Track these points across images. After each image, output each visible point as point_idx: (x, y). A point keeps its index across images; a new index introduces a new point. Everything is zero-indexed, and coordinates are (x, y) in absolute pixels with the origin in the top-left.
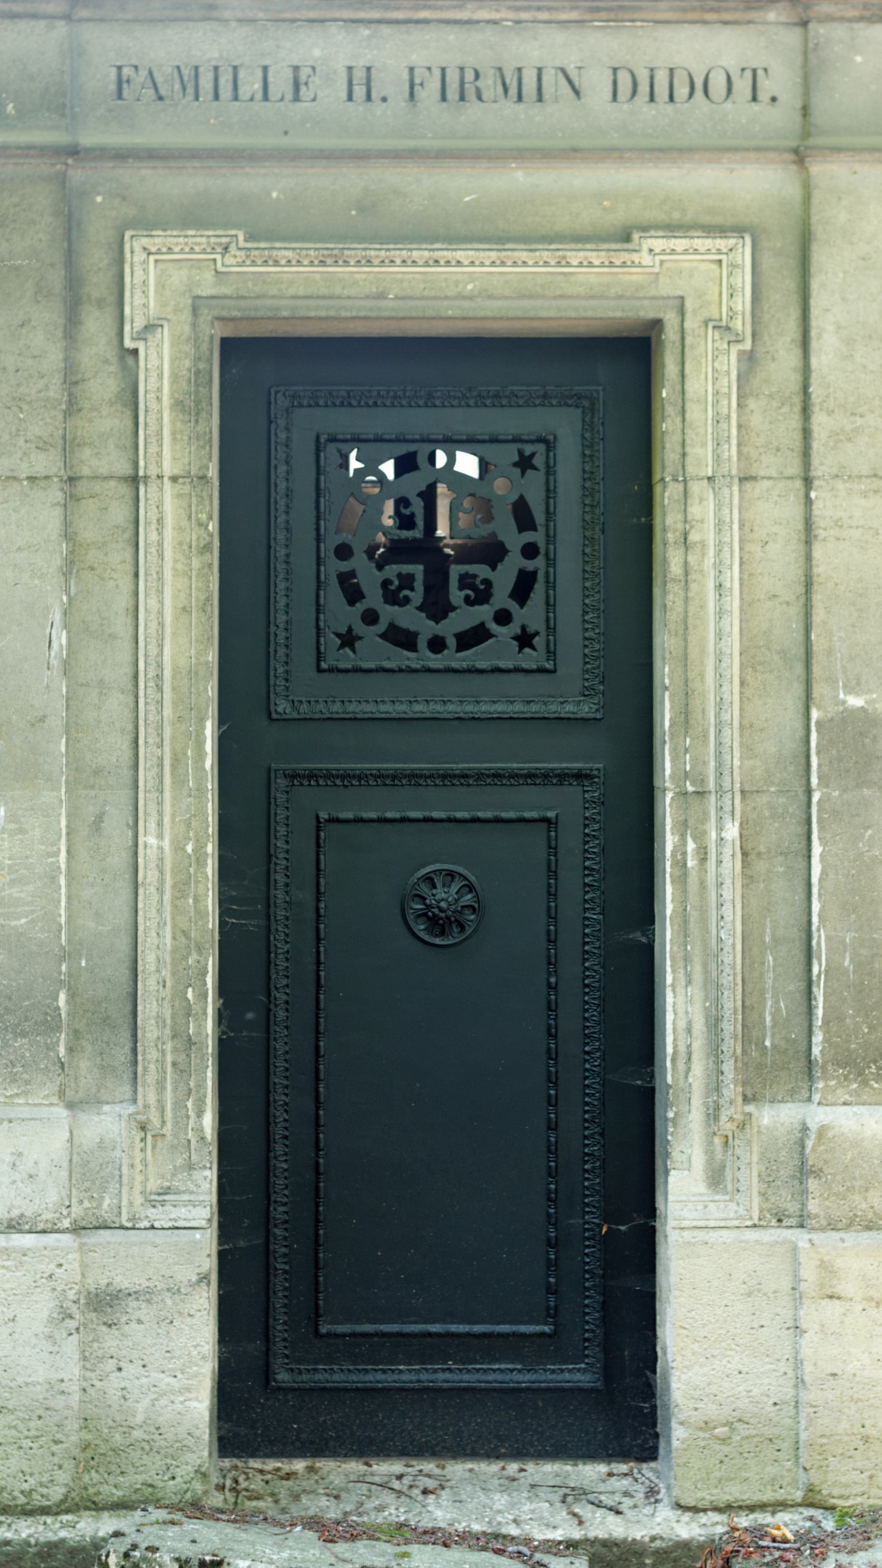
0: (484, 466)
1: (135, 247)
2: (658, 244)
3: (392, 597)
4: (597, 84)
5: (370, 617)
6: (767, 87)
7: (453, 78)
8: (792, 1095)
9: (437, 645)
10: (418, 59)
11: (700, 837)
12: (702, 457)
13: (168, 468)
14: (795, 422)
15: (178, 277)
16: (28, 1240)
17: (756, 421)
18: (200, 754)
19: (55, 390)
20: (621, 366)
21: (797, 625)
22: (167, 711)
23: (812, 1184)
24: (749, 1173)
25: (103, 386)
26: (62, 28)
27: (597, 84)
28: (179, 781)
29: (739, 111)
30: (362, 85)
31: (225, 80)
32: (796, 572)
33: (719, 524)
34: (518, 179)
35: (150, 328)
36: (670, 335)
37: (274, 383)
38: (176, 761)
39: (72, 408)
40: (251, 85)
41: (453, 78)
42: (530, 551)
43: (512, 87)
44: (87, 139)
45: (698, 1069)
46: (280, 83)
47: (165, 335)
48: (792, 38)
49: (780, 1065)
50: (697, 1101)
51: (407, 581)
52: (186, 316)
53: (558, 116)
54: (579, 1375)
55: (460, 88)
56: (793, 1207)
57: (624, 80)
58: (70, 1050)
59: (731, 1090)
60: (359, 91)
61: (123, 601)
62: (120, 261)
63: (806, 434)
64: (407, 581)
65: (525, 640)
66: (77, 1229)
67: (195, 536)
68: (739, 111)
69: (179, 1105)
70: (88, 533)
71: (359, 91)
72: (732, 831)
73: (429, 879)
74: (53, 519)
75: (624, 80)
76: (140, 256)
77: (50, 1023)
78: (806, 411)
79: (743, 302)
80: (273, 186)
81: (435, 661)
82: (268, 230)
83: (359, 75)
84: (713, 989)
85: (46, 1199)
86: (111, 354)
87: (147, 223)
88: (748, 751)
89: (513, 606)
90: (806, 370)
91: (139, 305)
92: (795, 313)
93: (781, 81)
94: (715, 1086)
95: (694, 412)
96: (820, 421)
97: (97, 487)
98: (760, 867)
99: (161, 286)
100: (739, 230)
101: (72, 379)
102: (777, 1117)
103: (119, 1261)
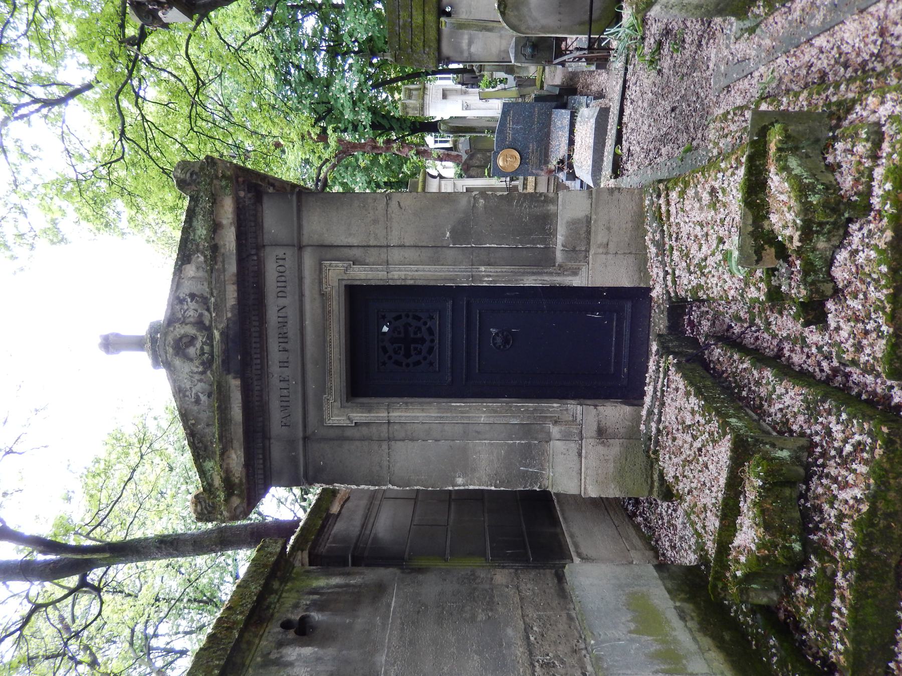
0: (385, 333)
1: (329, 423)
2: (324, 286)
3: (420, 353)
4: (282, 302)
5: (425, 358)
6: (281, 256)
7: (281, 340)
8: (554, 253)
9: (432, 341)
10: (276, 350)
11: (484, 276)
12: (382, 275)
13: (385, 414)
14: (372, 249)
15: (336, 411)
16: (583, 451)
17: (372, 260)
18: (460, 406)
19: (366, 443)
20: (358, 297)
21: (427, 249)
22: (449, 415)
23: (577, 249)
24: (574, 265)
25: (365, 431)
26: (272, 441)
27: (282, 302)
28: (467, 412)
29: (288, 263)
30: (284, 364)
31: (284, 399)
32: (413, 249)
33: (399, 270)
34: (308, 322)
35: (349, 419)
36: (349, 283)
37: (362, 385)
38: (462, 412)
39: (370, 439)
40: (285, 392)
41: (281, 340)
42: (407, 316)
43: (283, 324)
44: (301, 434)
45: (546, 278)
46: (283, 385)
47: (352, 415)
48: (268, 250)
49: (545, 260)
50: (555, 278)
51: (415, 349)
52: (346, 410)
53: (292, 314)
54: (628, 306)
55: (283, 337)
56: (583, 254)
57: (280, 294)
58: (536, 439)
59: (551, 270)
60: (286, 364)
61: (420, 426)
62: (332, 426)
63: (374, 246)
64: (415, 349)
65: (431, 318)
66: (582, 440)
67: (404, 407)
68: (288, 263)
69: (551, 412)
70: (403, 435)
71: (286, 364)
72: (483, 268)
73: (495, 344)
74: (400, 443)
75: (280, 294)
76: (331, 421)
77: (529, 445)
78: (369, 246)
79: (340, 264)
80: (311, 386)
81: (437, 341)
82: (323, 389)
83: (282, 364)
84: (524, 273)
85: (573, 446)
86: (356, 428)
87: (322, 420)
88: (461, 263)
89: (422, 321)
90: (358, 246)
91: (345, 423)
92: (342, 249)
93: (280, 252)
94: (551, 274)
95: (370, 277)
96: (371, 243)
97: (391, 432)
98: (492, 260)
99: (338, 416)
100: (321, 264)
101: (363, 439)
102: (559, 256)
103: (590, 429)
